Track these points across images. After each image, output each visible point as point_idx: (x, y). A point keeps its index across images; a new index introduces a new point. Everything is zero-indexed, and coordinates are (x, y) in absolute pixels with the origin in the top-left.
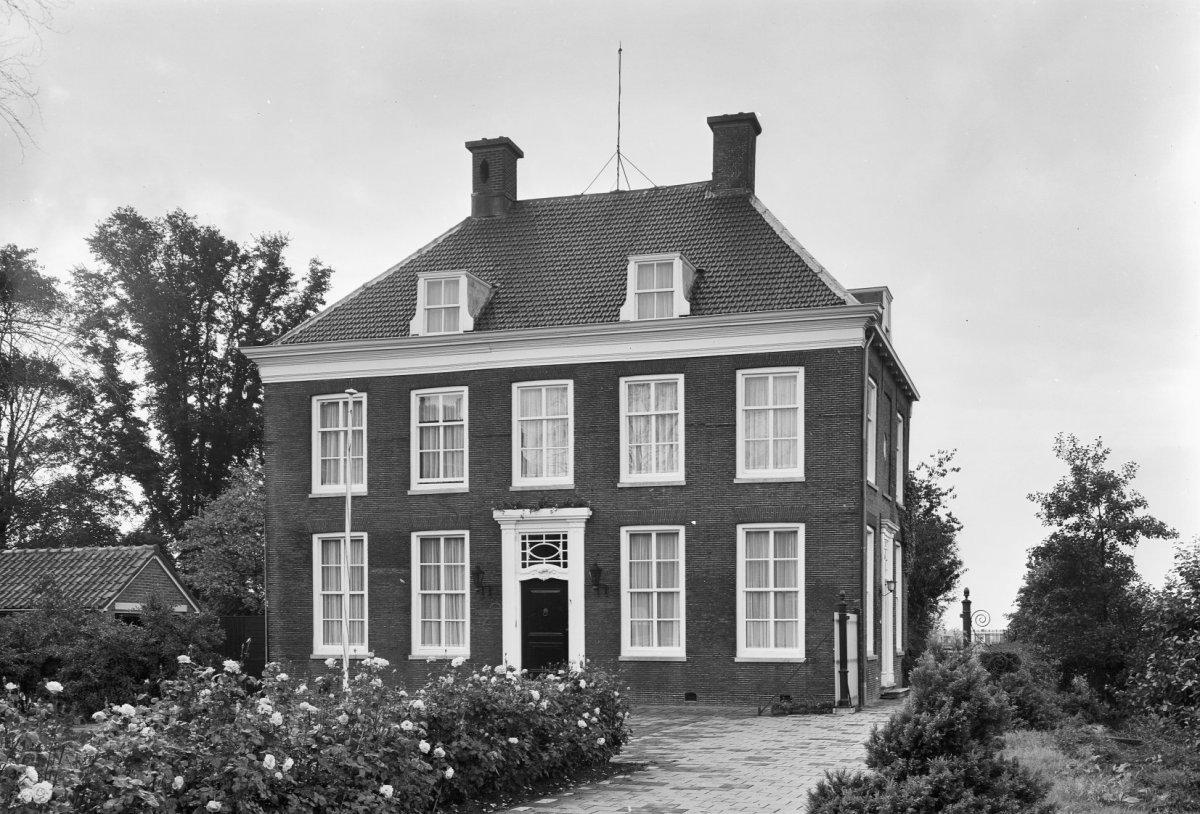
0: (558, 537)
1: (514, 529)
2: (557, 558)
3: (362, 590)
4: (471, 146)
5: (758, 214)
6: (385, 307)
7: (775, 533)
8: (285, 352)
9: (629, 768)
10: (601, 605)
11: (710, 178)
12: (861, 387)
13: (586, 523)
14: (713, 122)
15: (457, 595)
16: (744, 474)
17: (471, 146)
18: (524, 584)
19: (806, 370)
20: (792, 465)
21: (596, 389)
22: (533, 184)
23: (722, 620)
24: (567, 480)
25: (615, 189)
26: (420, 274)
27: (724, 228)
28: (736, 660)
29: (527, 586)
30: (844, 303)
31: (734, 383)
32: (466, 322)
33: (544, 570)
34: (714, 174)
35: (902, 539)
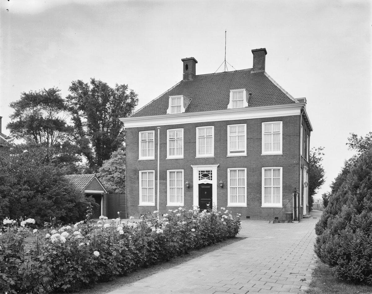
0: (209, 171)
1: (196, 170)
2: (209, 177)
3: (244, 185)
4: (183, 60)
5: (267, 77)
6: (159, 107)
7: (238, 170)
8: (131, 119)
9: (237, 238)
10: (222, 191)
11: (252, 68)
12: (299, 127)
13: (217, 167)
14: (253, 51)
15: (234, 188)
16: (264, 153)
17: (183, 60)
18: (199, 185)
19: (283, 122)
20: (269, 150)
21: (221, 129)
22: (200, 70)
23: (257, 195)
24: (211, 154)
25: (224, 71)
26: (170, 97)
27: (257, 82)
28: (262, 207)
29: (200, 185)
30: (295, 102)
31: (261, 126)
32: (183, 110)
33: (205, 181)
34: (253, 66)
35: (308, 172)
